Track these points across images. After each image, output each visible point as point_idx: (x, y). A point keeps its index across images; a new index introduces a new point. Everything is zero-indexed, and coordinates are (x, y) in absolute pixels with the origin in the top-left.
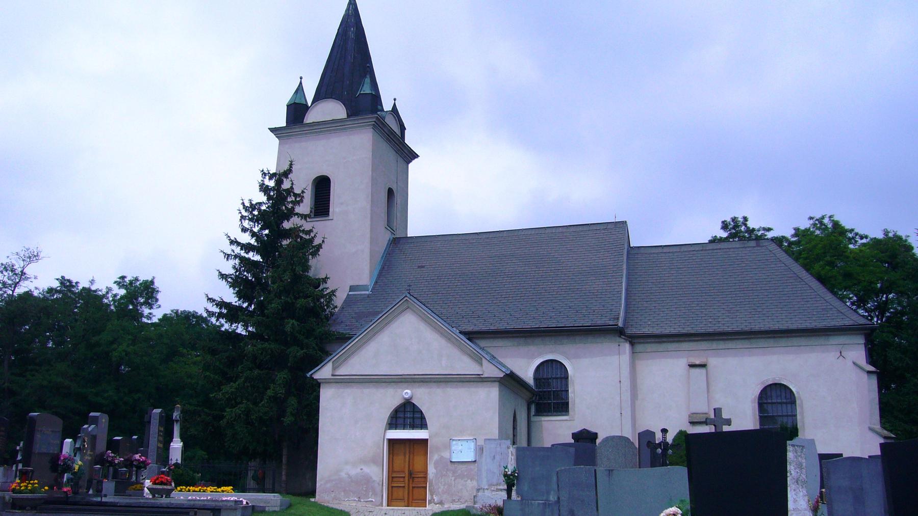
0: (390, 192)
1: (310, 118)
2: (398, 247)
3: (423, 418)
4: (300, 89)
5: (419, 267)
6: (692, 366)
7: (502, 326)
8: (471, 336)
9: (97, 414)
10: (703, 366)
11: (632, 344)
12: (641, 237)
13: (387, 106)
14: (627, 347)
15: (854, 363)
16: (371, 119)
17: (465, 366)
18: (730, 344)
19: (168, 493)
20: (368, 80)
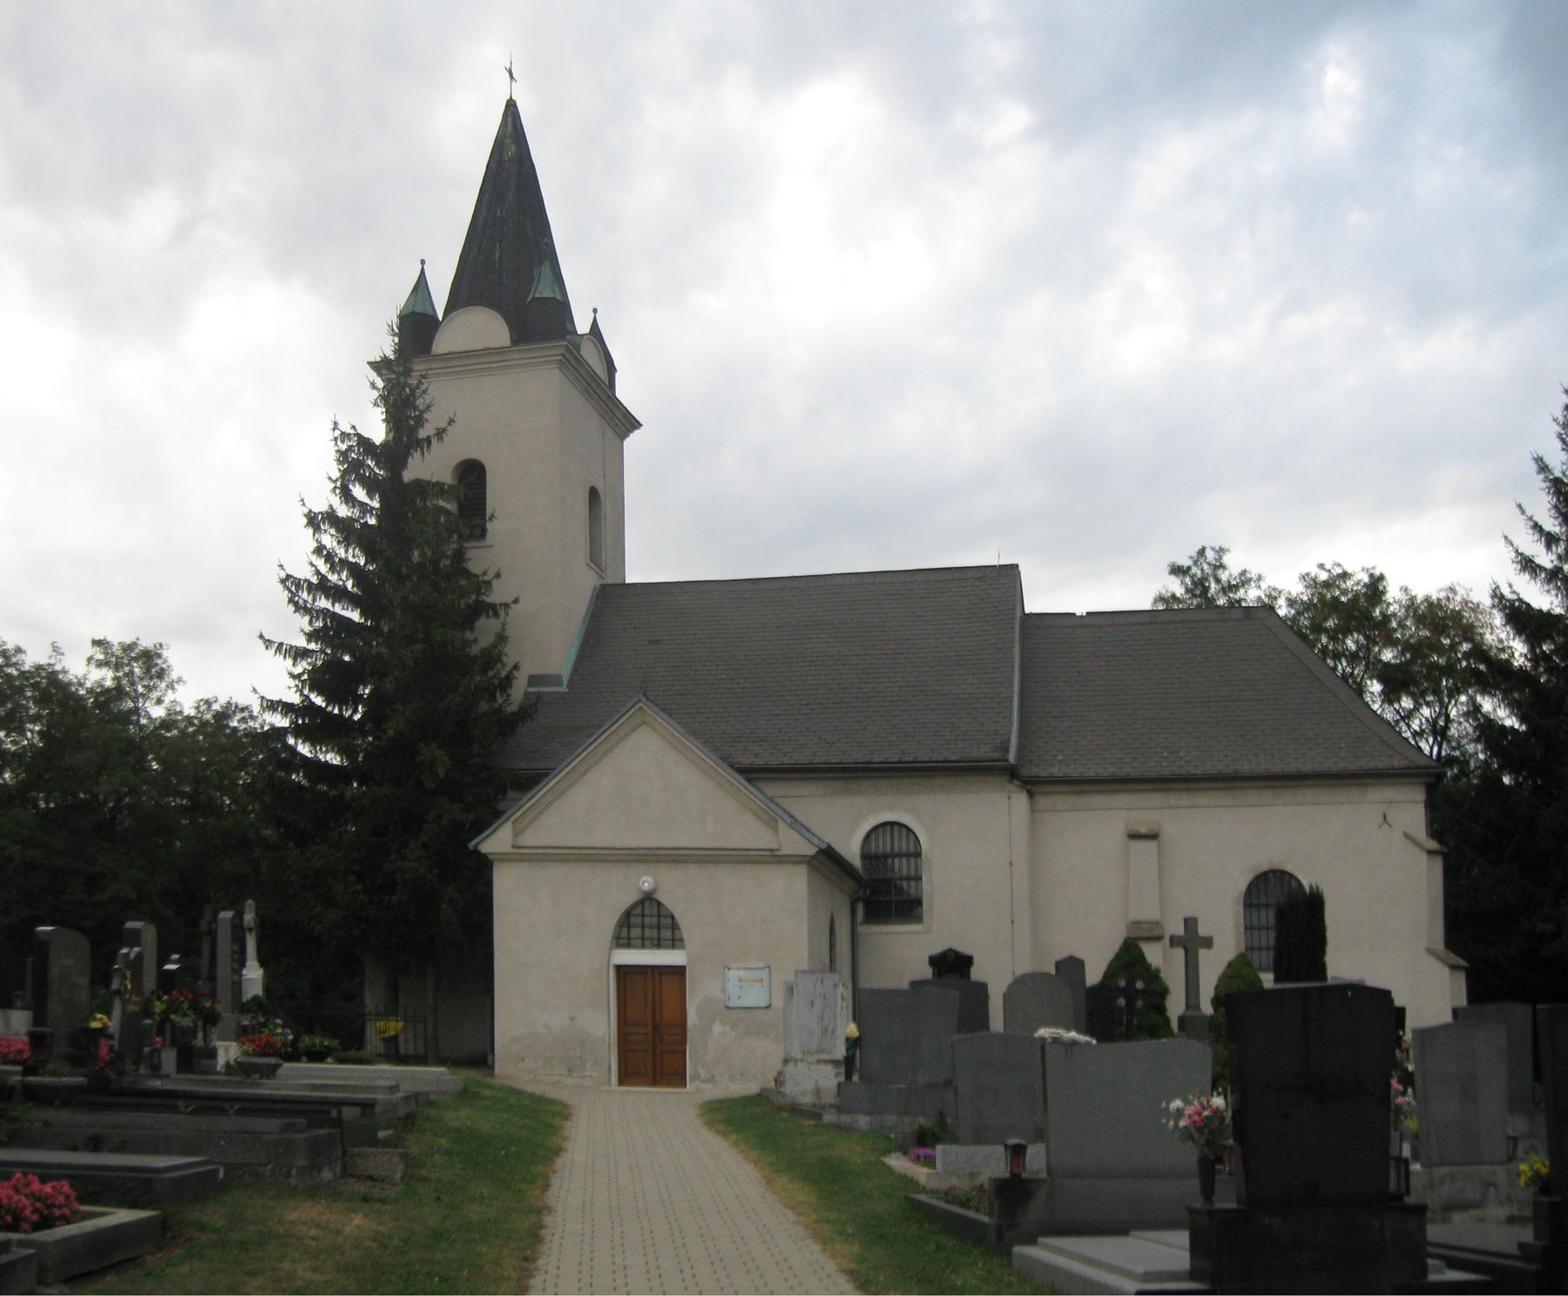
0: (593, 494)
1: (443, 343)
2: (616, 602)
3: (674, 926)
4: (421, 286)
5: (651, 642)
6: (1134, 836)
7: (802, 758)
8: (752, 774)
9: (138, 925)
10: (1153, 836)
11: (1031, 795)
12: (1047, 594)
13: (582, 327)
14: (1020, 800)
15: (1407, 836)
16: (555, 349)
17: (748, 832)
18: (1201, 799)
19: (271, 1071)
20: (546, 269)
